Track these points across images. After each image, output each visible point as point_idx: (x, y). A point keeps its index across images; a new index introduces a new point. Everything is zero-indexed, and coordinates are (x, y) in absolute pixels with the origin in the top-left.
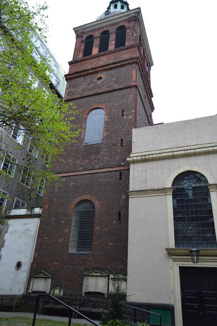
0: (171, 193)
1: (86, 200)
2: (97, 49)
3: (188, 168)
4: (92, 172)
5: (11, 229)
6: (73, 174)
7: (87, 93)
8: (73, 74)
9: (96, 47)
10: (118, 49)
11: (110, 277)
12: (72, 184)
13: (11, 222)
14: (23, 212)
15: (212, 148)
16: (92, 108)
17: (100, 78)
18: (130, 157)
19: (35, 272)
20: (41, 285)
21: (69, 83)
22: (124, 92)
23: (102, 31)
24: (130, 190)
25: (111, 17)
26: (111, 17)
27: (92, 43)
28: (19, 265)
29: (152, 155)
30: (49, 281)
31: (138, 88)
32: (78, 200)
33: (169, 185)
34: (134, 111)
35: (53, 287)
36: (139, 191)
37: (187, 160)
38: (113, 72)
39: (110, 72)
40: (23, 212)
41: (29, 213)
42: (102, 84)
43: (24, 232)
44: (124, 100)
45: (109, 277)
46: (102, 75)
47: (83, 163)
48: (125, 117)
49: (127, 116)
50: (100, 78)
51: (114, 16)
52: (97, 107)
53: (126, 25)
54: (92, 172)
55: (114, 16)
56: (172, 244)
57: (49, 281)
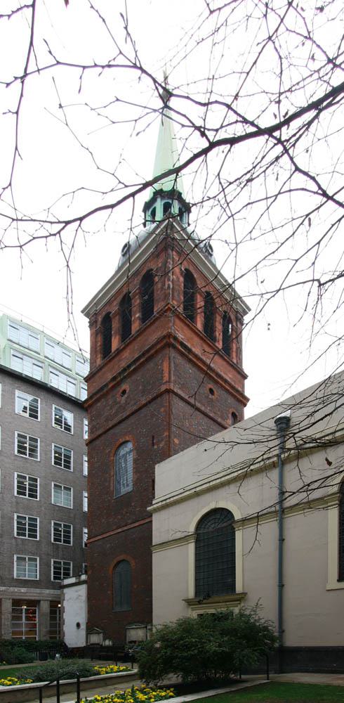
0: (337, 502)
1: (123, 560)
2: (117, 337)
3: (213, 506)
4: (125, 528)
5: (67, 597)
6: (108, 534)
7: (111, 424)
8: (95, 394)
9: (115, 333)
10: (128, 341)
11: (148, 628)
12: (108, 546)
13: (66, 590)
14: (72, 580)
15: (208, 485)
16: (118, 443)
17: (124, 392)
18: (152, 504)
19: (90, 630)
20: (95, 639)
21: (90, 413)
22: (152, 407)
23: (140, 278)
24: (153, 544)
25: (136, 251)
26: (136, 251)
27: (111, 329)
28: (78, 625)
29: (170, 498)
30: (101, 635)
31: (173, 392)
32: (115, 562)
33: (192, 529)
34: (166, 434)
35: (104, 640)
36: (160, 544)
37: (324, 452)
38: (137, 376)
39: (134, 377)
40: (72, 580)
41: (77, 581)
42: (126, 401)
43: (77, 598)
44: (154, 419)
45: (146, 627)
46: (124, 386)
47: (116, 520)
48: (155, 447)
49: (159, 442)
50: (124, 392)
51: (140, 246)
52: (124, 440)
53: (153, 266)
54: (125, 528)
55: (140, 246)
56: (191, 593)
57: (101, 635)
